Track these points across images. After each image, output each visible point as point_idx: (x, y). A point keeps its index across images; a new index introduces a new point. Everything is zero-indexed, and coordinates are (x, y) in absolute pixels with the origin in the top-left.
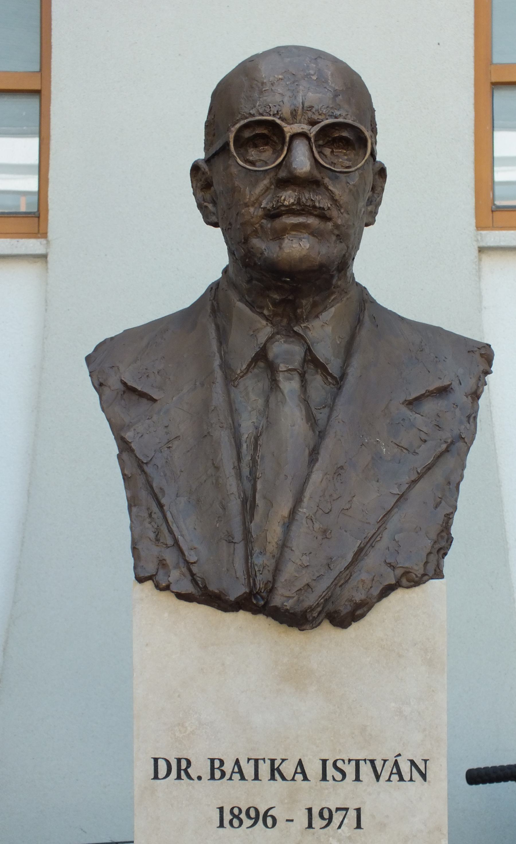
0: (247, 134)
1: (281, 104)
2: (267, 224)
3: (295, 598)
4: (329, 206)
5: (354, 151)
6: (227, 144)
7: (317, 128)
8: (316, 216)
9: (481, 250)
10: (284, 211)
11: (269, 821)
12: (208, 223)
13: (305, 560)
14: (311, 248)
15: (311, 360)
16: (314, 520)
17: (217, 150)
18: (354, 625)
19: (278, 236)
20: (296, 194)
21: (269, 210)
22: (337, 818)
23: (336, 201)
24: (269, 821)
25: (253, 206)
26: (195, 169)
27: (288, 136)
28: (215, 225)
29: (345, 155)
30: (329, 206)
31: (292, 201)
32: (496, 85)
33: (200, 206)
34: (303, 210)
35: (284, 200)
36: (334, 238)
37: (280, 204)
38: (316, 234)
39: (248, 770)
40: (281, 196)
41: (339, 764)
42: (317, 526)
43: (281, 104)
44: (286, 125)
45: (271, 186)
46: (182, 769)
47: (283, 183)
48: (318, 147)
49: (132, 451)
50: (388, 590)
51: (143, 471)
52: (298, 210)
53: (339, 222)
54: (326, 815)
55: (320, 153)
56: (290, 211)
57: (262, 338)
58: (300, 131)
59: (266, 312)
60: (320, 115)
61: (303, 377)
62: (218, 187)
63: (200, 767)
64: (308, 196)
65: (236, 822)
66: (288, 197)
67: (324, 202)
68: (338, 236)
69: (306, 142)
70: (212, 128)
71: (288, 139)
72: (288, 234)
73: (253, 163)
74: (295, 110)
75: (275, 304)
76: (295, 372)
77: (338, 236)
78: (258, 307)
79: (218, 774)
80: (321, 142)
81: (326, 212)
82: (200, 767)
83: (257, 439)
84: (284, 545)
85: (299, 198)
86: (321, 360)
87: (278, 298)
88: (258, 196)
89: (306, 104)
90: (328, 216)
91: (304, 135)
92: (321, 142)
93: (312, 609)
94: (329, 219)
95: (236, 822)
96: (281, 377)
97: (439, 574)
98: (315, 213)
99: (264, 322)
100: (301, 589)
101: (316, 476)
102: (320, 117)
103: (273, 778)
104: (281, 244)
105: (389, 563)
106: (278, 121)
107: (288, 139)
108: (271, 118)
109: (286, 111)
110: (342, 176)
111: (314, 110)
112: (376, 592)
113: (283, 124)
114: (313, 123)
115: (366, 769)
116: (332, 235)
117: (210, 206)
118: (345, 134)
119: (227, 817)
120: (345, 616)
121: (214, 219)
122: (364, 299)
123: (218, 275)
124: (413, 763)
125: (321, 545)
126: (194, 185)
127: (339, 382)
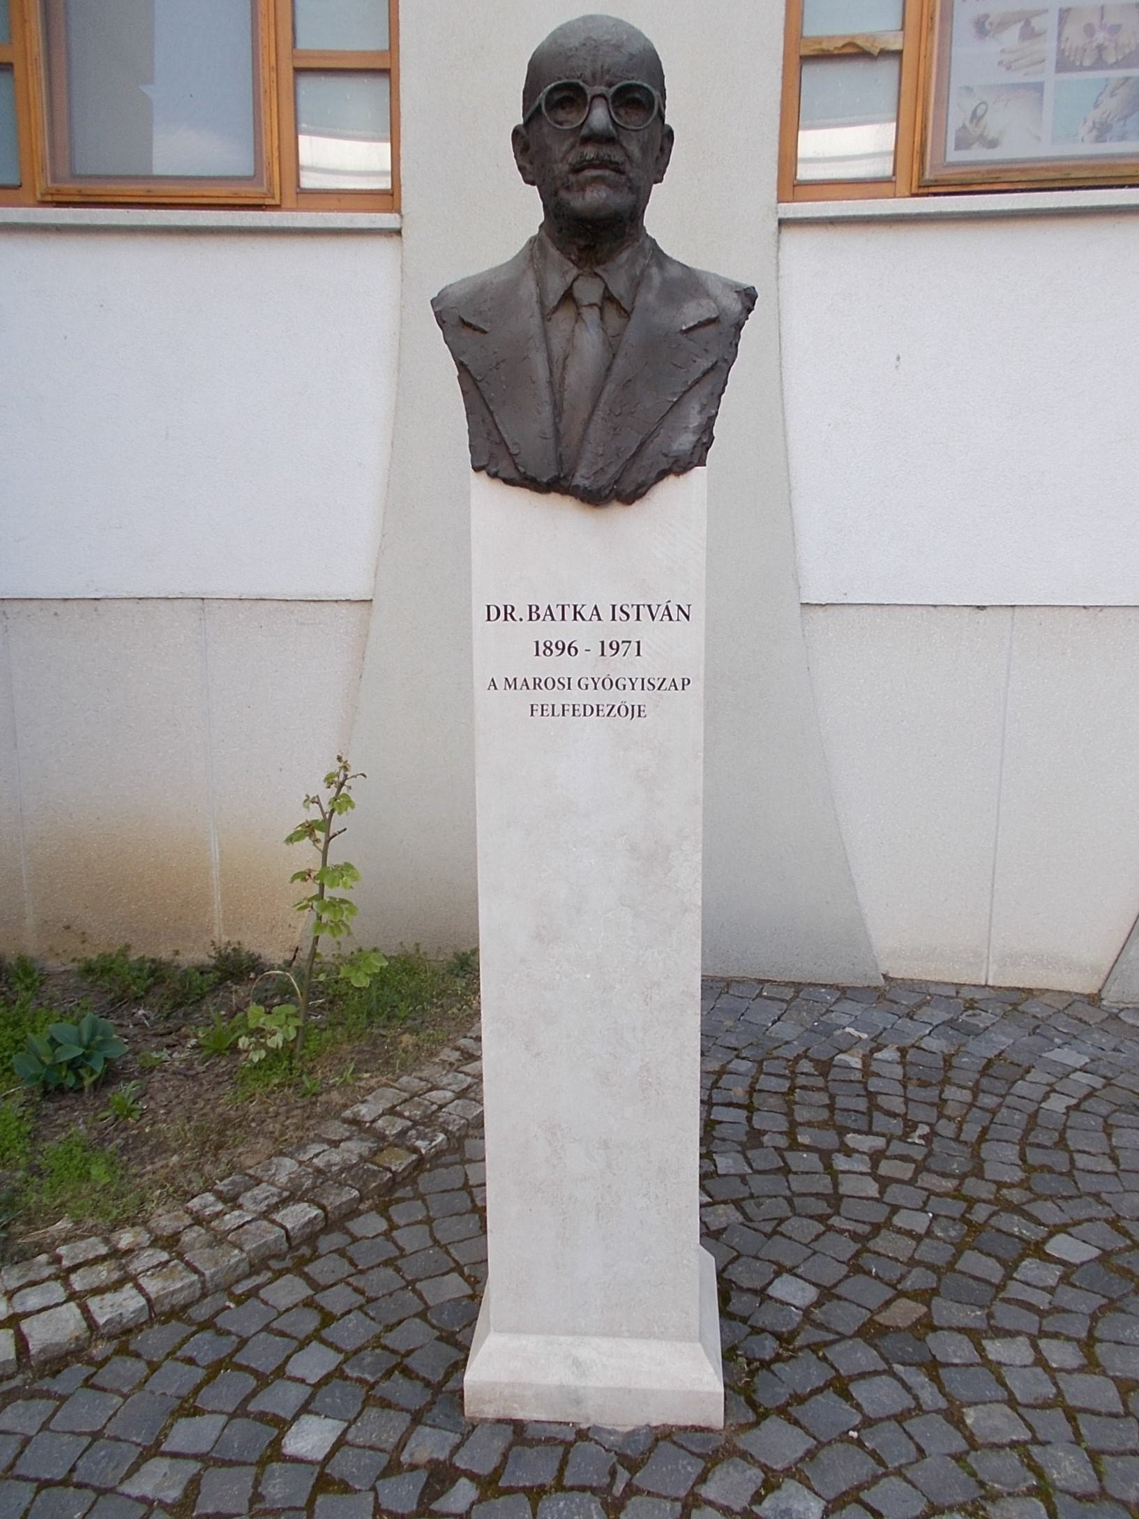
0: (557, 97)
2: (572, 178)
6: (540, 106)
9: (782, 223)
11: (573, 650)
12: (526, 182)
13: (600, 450)
14: (607, 198)
15: (608, 297)
17: (532, 115)
18: (637, 503)
19: (583, 189)
22: (623, 647)
24: (573, 650)
26: (516, 133)
27: (589, 97)
28: (533, 183)
32: (805, 59)
33: (520, 168)
38: (613, 186)
39: (557, 613)
41: (625, 608)
42: (609, 424)
46: (508, 613)
47: (586, 140)
49: (468, 371)
51: (478, 388)
54: (615, 646)
55: (616, 113)
56: (591, 165)
57: (569, 279)
59: (573, 257)
61: (601, 309)
62: (533, 148)
63: (521, 612)
64: (606, 151)
65: (548, 652)
66: (590, 152)
67: (618, 156)
70: (530, 92)
73: (561, 124)
75: (580, 250)
79: (534, 616)
82: (521, 612)
84: (583, 438)
88: (562, 153)
89: (606, 67)
91: (602, 96)
93: (604, 487)
94: (621, 172)
95: (548, 652)
101: (610, 387)
103: (575, 619)
106: (582, 84)
108: (574, 81)
109: (588, 73)
110: (633, 134)
112: (653, 475)
113: (585, 86)
114: (610, 85)
115: (644, 612)
117: (528, 166)
118: (637, 95)
119: (542, 648)
120: (631, 494)
121: (531, 178)
122: (659, 257)
123: (536, 231)
124: (679, 607)
127: (626, 314)
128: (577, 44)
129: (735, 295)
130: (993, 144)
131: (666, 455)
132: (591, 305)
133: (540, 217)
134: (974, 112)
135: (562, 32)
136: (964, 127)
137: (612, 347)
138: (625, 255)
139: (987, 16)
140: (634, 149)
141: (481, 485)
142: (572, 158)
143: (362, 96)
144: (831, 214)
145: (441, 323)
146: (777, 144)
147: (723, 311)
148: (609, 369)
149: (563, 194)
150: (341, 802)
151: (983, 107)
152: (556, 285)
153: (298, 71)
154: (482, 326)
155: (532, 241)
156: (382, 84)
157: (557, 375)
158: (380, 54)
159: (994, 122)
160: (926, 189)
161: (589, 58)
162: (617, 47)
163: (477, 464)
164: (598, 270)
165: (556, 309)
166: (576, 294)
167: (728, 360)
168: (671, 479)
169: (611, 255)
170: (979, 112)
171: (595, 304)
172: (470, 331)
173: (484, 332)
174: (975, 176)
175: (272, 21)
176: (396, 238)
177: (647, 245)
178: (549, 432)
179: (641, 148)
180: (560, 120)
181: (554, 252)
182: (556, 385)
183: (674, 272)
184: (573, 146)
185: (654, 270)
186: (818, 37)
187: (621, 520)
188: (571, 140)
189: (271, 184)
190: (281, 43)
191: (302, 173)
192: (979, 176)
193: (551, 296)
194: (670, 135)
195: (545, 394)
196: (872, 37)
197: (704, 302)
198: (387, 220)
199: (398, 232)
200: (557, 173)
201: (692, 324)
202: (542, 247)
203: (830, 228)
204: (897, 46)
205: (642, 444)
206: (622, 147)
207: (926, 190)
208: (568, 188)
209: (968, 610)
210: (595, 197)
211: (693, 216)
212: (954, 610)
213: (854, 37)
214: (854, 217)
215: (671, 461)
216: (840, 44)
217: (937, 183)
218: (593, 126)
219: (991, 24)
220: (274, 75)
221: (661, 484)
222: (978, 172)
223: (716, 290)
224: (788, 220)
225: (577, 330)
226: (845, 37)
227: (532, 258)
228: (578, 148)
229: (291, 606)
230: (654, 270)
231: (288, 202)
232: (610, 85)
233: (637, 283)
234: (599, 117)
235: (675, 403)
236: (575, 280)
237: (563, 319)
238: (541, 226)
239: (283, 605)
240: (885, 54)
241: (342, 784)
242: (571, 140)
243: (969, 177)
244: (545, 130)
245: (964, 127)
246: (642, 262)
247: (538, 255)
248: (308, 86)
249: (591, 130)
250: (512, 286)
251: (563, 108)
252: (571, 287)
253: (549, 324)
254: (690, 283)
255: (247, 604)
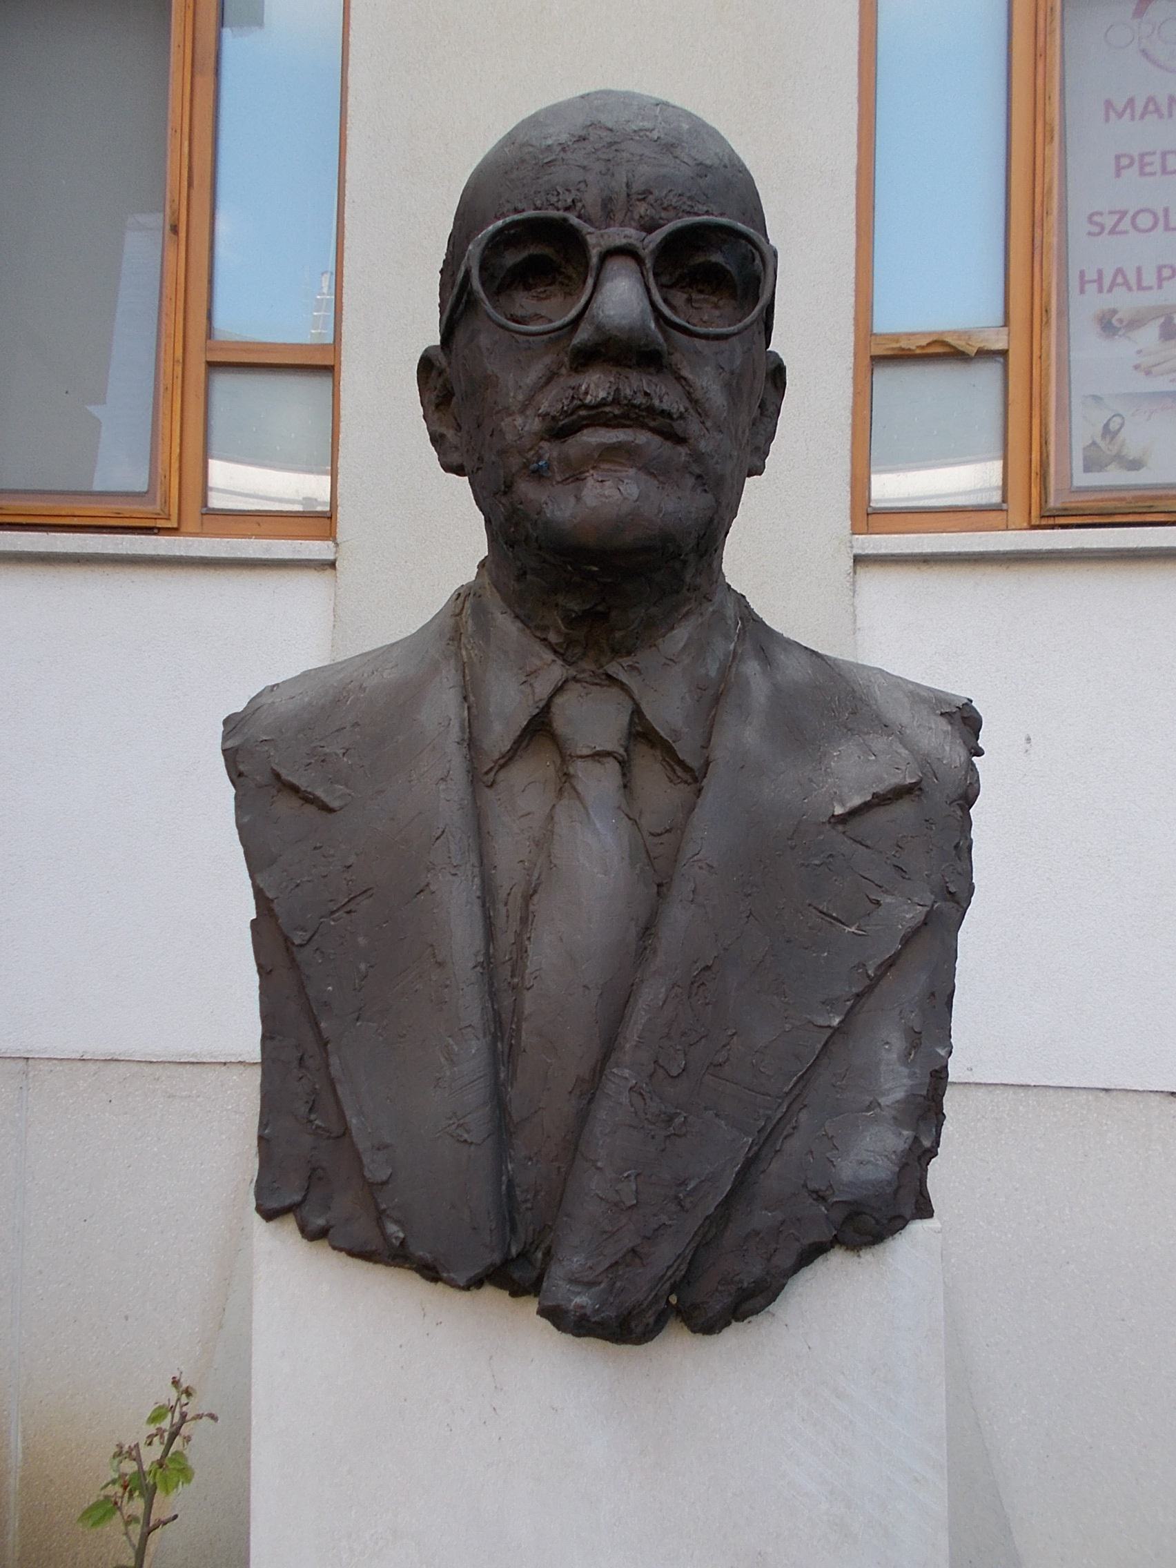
0: (512, 258)
1: (582, 186)
2: (550, 451)
3: (602, 1286)
4: (682, 409)
5: (733, 302)
7: (658, 236)
8: (655, 431)
10: (584, 418)
12: (448, 468)
15: (642, 733)
16: (647, 1096)
17: (458, 308)
19: (575, 475)
20: (612, 379)
21: (553, 418)
23: (696, 402)
25: (522, 411)
26: (426, 365)
27: (594, 254)
28: (459, 470)
29: (716, 307)
30: (682, 409)
31: (602, 394)
32: (878, 360)
33: (434, 440)
34: (625, 416)
35: (586, 393)
36: (690, 481)
37: (576, 402)
38: (654, 470)
40: (580, 386)
43: (582, 186)
44: (591, 229)
45: (559, 368)
47: (585, 358)
48: (661, 287)
50: (811, 1254)
52: (615, 416)
53: (703, 446)
56: (597, 416)
57: (543, 688)
58: (620, 241)
59: (553, 637)
60: (665, 209)
61: (625, 765)
64: (636, 384)
66: (596, 385)
67: (668, 397)
68: (699, 477)
69: (631, 264)
71: (594, 261)
72: (594, 468)
74: (611, 199)
75: (571, 621)
76: (611, 759)
77: (699, 477)
78: (537, 627)
80: (665, 279)
81: (675, 424)
83: (528, 897)
85: (618, 390)
86: (662, 733)
87: (576, 608)
88: (526, 393)
89: (637, 187)
90: (680, 432)
92: (665, 279)
96: (579, 769)
97: (924, 1209)
98: (652, 424)
99: (549, 656)
100: (617, 1263)
102: (663, 214)
104: (580, 490)
105: (813, 1192)
106: (574, 220)
107: (594, 261)
108: (552, 213)
109: (591, 198)
111: (651, 198)
112: (784, 1260)
113: (585, 228)
114: (649, 227)
116: (687, 475)
117: (450, 434)
121: (455, 458)
125: (663, 1150)
126: (426, 402)
127: (692, 776)
128: (564, 138)
129: (944, 725)
130: (1135, 465)
131: (820, 1197)
132: (598, 756)
133: (479, 546)
134: (1106, 426)
135: (533, 122)
136: (1094, 443)
137: (658, 866)
138: (681, 635)
139: (1114, 312)
140: (709, 384)
141: (278, 1252)
142: (548, 402)
143: (294, 400)
144: (928, 550)
145: (236, 775)
146: (848, 460)
147: (925, 761)
148: (648, 930)
149: (527, 489)
150: (173, 1467)
151: (1118, 420)
152: (510, 702)
153: (212, 366)
154: (320, 793)
155: (462, 595)
156: (318, 386)
157: (506, 940)
158: (323, 347)
159: (1133, 440)
160: (1051, 519)
161: (599, 166)
162: (669, 147)
163: (274, 1204)
164: (613, 669)
165: (508, 759)
166: (560, 724)
167: (955, 895)
168: (837, 1260)
169: (651, 630)
170: (1114, 426)
171: (609, 754)
172: (296, 802)
173: (326, 808)
174: (1118, 504)
175: (181, 304)
176: (329, 572)
177: (731, 611)
178: (478, 1123)
179: (727, 386)
180: (519, 312)
181: (506, 625)
182: (501, 974)
183: (794, 670)
184: (551, 377)
185: (752, 668)
186: (894, 334)
187: (694, 1372)
188: (547, 360)
189: (166, 501)
190: (191, 332)
191: (210, 494)
192: (1124, 504)
193: (498, 727)
194: (777, 375)
195: (470, 1005)
196: (967, 334)
197: (879, 743)
198: (317, 549)
199: (332, 565)
200: (510, 437)
201: (856, 801)
202: (480, 612)
203: (924, 568)
204: (1000, 345)
205: (750, 1163)
206: (680, 378)
207: (1051, 521)
208: (538, 475)
209: (1158, 1097)
210: (607, 496)
211: (834, 549)
212: (1137, 1096)
213: (943, 333)
214: (959, 554)
215: (838, 1215)
216: (924, 342)
217: (1065, 513)
218: (606, 319)
219: (1121, 321)
220: (179, 369)
221: (806, 1273)
222: (1123, 499)
223: (900, 714)
224: (867, 556)
225: (561, 816)
226: (930, 334)
227: (456, 636)
228: (567, 380)
229: (158, 1071)
230: (752, 668)
231: (190, 523)
232: (649, 227)
233: (715, 698)
234: (621, 298)
235: (836, 1030)
236: (559, 690)
237: (526, 787)
238: (482, 565)
239: (147, 1069)
240: (985, 354)
241: (174, 1435)
242: (547, 360)
243: (1110, 505)
244: (484, 340)
245: (1094, 443)
246: (722, 647)
247: (470, 627)
248: (224, 383)
249: (599, 328)
250: (405, 698)
251: (528, 288)
252: (546, 709)
253: (490, 793)
254: (834, 699)
255: (92, 1067)
